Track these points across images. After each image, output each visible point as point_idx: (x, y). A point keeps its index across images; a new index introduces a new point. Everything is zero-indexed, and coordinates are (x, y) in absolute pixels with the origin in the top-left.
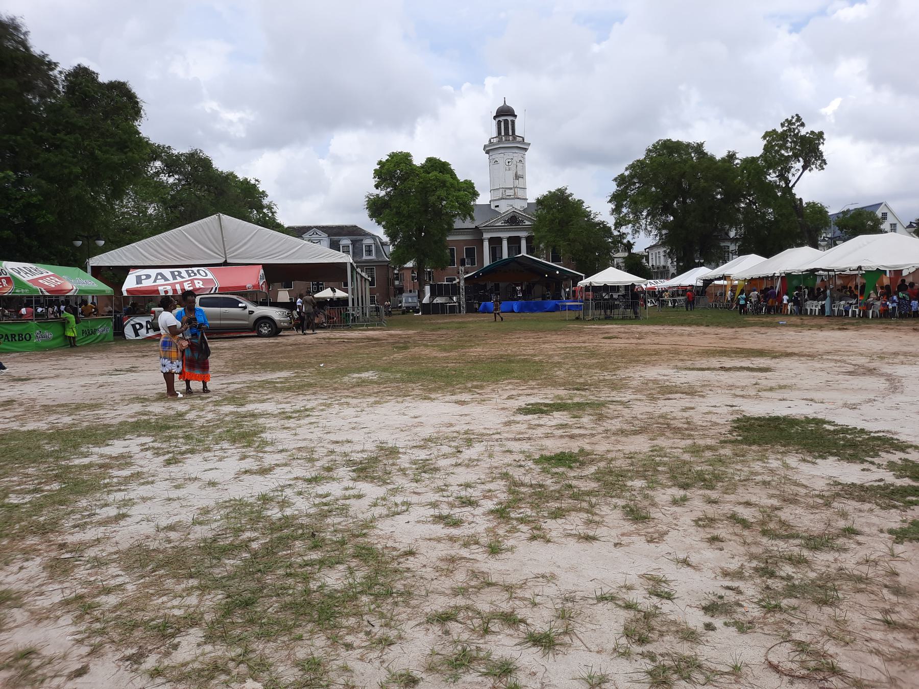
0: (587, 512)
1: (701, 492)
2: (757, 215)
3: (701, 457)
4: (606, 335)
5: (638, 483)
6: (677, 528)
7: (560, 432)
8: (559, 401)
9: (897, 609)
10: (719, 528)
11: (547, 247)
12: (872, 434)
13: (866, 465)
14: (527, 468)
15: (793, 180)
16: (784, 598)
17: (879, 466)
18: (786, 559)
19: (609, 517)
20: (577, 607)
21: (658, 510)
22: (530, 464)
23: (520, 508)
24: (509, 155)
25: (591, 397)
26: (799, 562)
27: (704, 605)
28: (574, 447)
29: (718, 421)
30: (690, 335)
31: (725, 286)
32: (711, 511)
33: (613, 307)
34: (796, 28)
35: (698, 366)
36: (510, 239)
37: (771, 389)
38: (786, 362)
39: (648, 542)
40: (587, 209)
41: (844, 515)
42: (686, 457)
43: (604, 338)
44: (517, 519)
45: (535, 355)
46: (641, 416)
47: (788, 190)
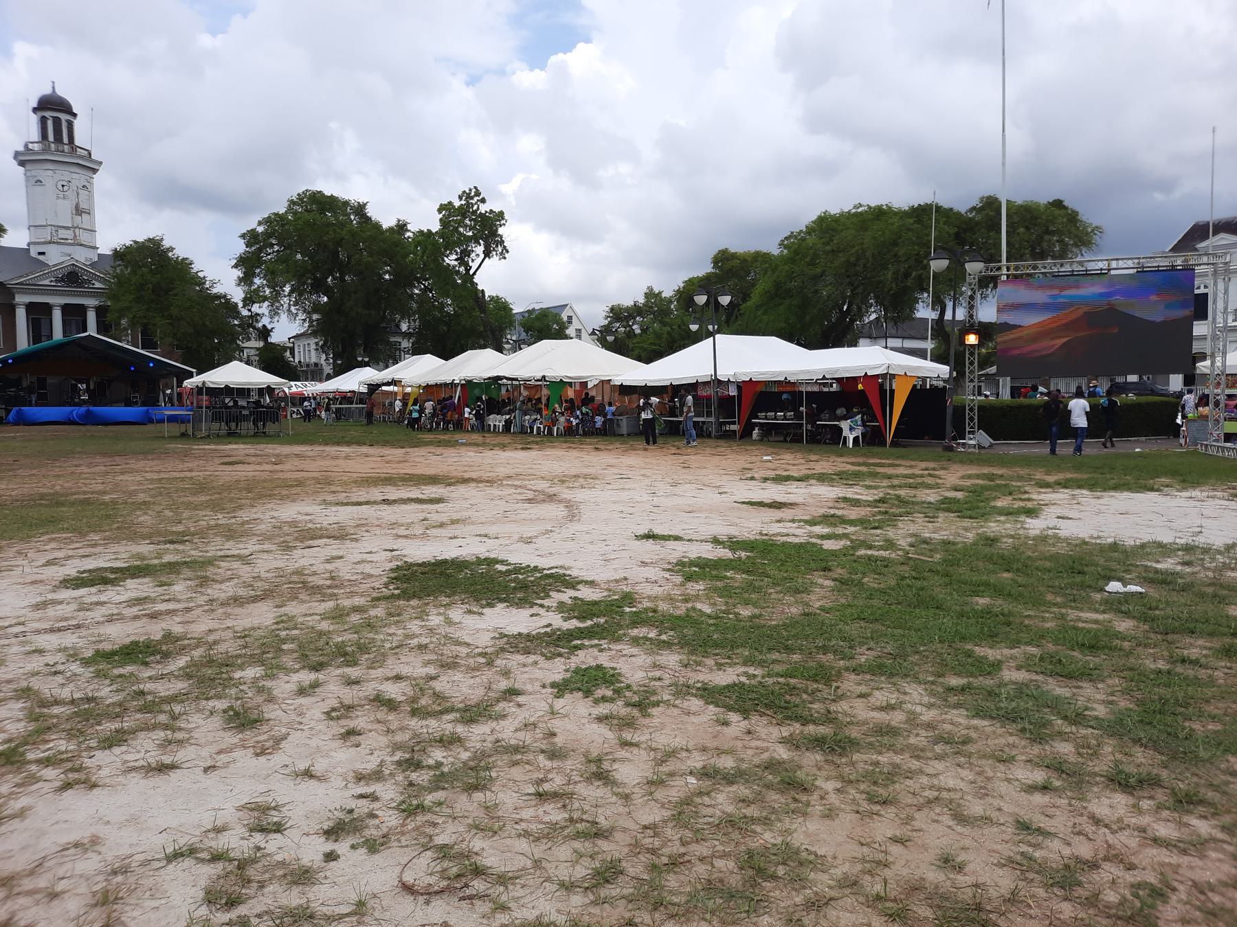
0: (166, 727)
1: (338, 672)
2: (434, 305)
3: (344, 623)
4: (227, 459)
5: (251, 672)
6: (301, 727)
7: (134, 610)
8: (138, 563)
9: (550, 776)
10: (357, 716)
11: (133, 324)
12: (545, 572)
13: (535, 610)
14: (68, 674)
15: (474, 266)
16: (430, 793)
17: (548, 609)
18: (436, 741)
19: (202, 729)
20: (132, 879)
21: (277, 706)
22: (75, 667)
23: (47, 741)
24: (64, 174)
25: (193, 552)
26: (451, 743)
27: (326, 828)
28: (155, 630)
29: (372, 572)
30: (347, 457)
31: (396, 393)
32: (349, 695)
33: (238, 419)
34: (472, 81)
35: (354, 499)
36: (66, 309)
37: (442, 525)
38: (461, 490)
39: (257, 755)
40: (201, 275)
41: (506, 673)
42: (325, 626)
43: (222, 464)
44: (39, 762)
45: (105, 493)
46: (267, 575)
47: (469, 278)
